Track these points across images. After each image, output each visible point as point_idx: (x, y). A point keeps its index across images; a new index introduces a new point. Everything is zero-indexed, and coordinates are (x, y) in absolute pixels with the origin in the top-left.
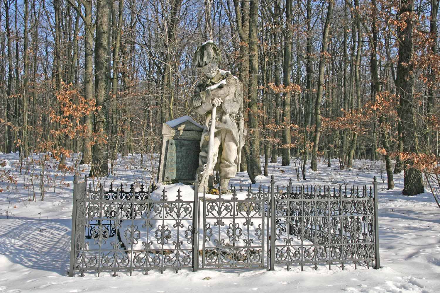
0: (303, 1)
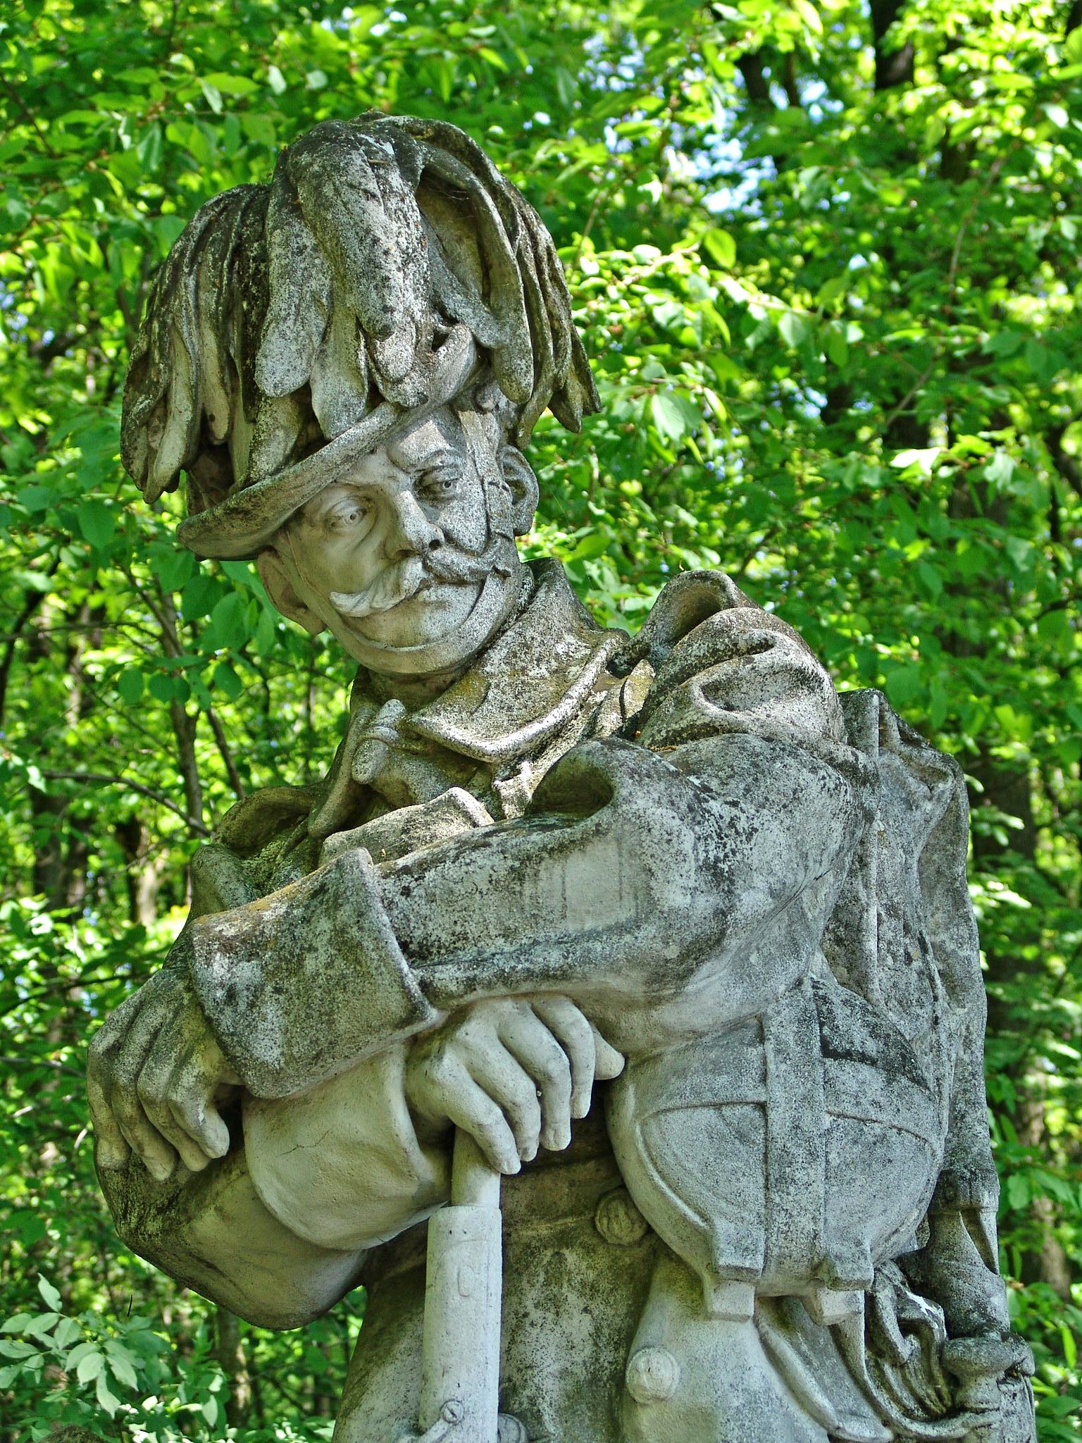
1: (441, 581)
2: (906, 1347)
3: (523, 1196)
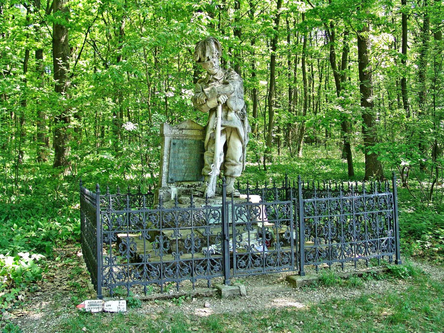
0: (1, 24)
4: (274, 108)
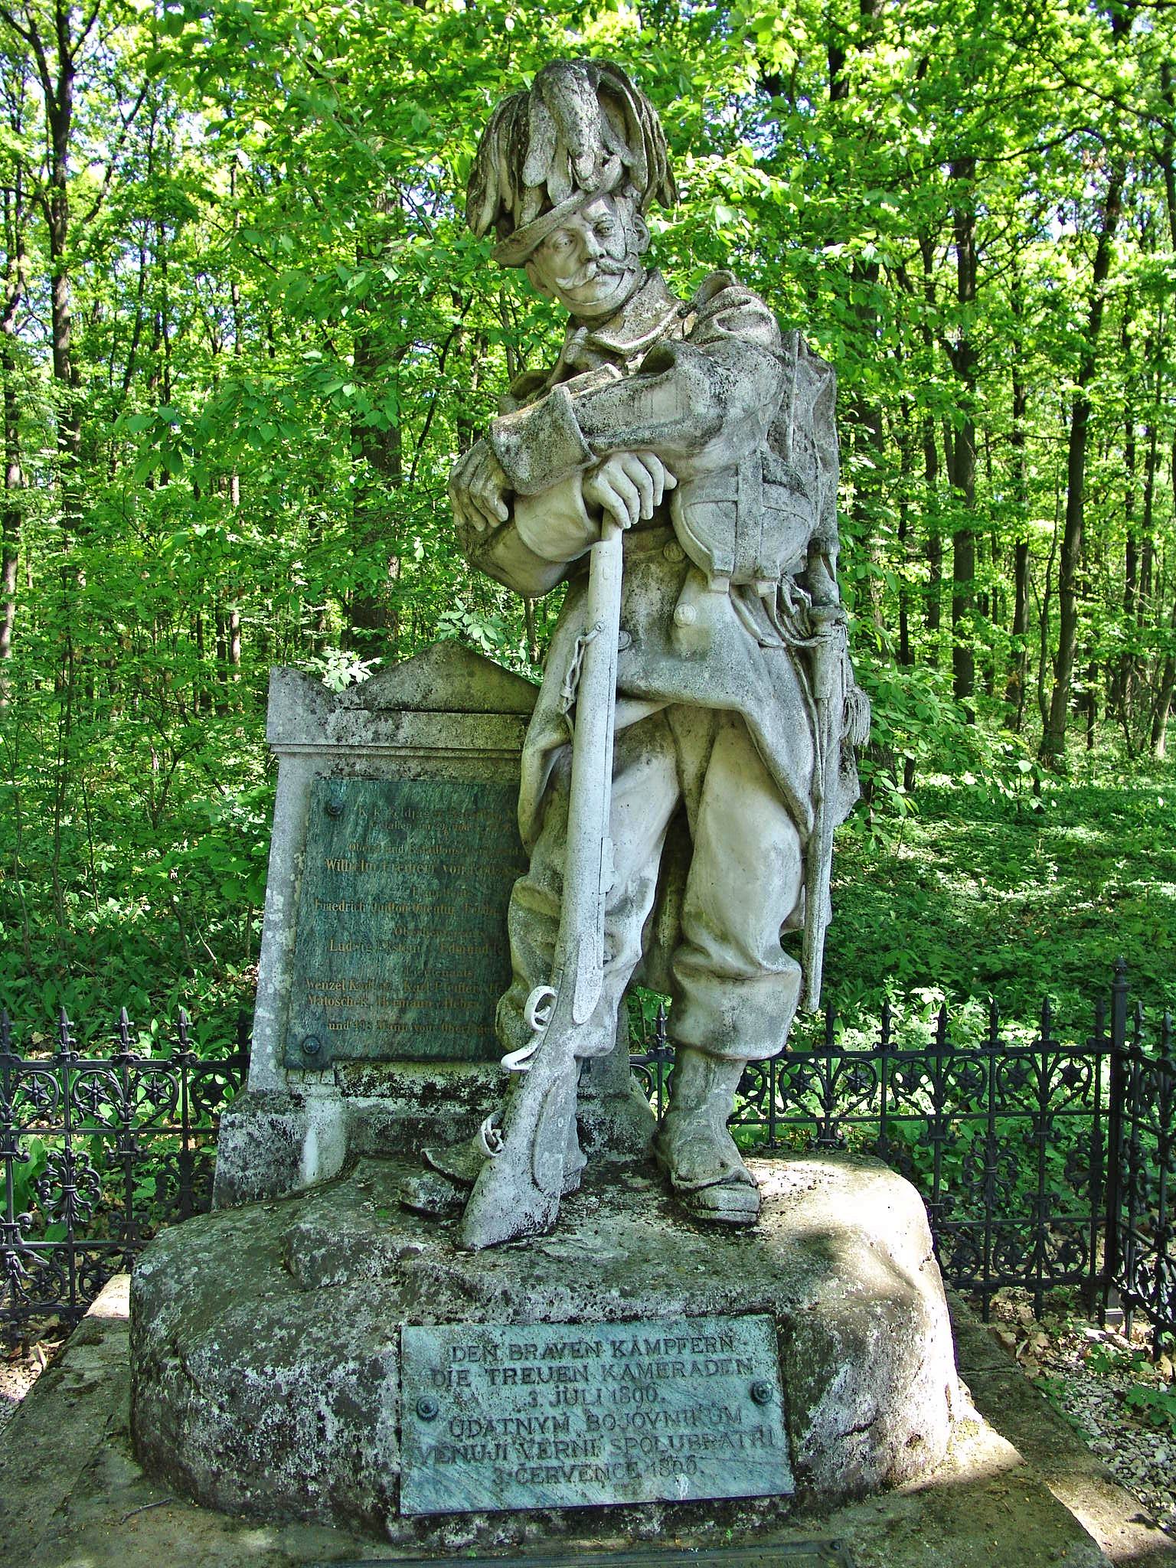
1: (604, 273)
2: (794, 609)
3: (634, 540)
4: (1077, 604)
